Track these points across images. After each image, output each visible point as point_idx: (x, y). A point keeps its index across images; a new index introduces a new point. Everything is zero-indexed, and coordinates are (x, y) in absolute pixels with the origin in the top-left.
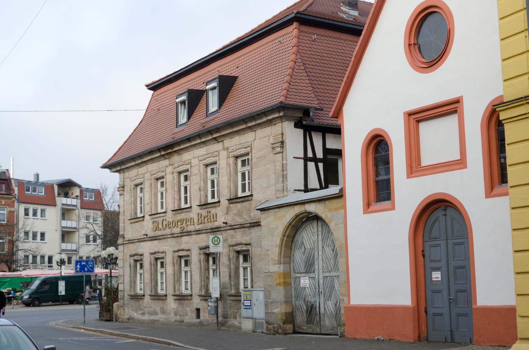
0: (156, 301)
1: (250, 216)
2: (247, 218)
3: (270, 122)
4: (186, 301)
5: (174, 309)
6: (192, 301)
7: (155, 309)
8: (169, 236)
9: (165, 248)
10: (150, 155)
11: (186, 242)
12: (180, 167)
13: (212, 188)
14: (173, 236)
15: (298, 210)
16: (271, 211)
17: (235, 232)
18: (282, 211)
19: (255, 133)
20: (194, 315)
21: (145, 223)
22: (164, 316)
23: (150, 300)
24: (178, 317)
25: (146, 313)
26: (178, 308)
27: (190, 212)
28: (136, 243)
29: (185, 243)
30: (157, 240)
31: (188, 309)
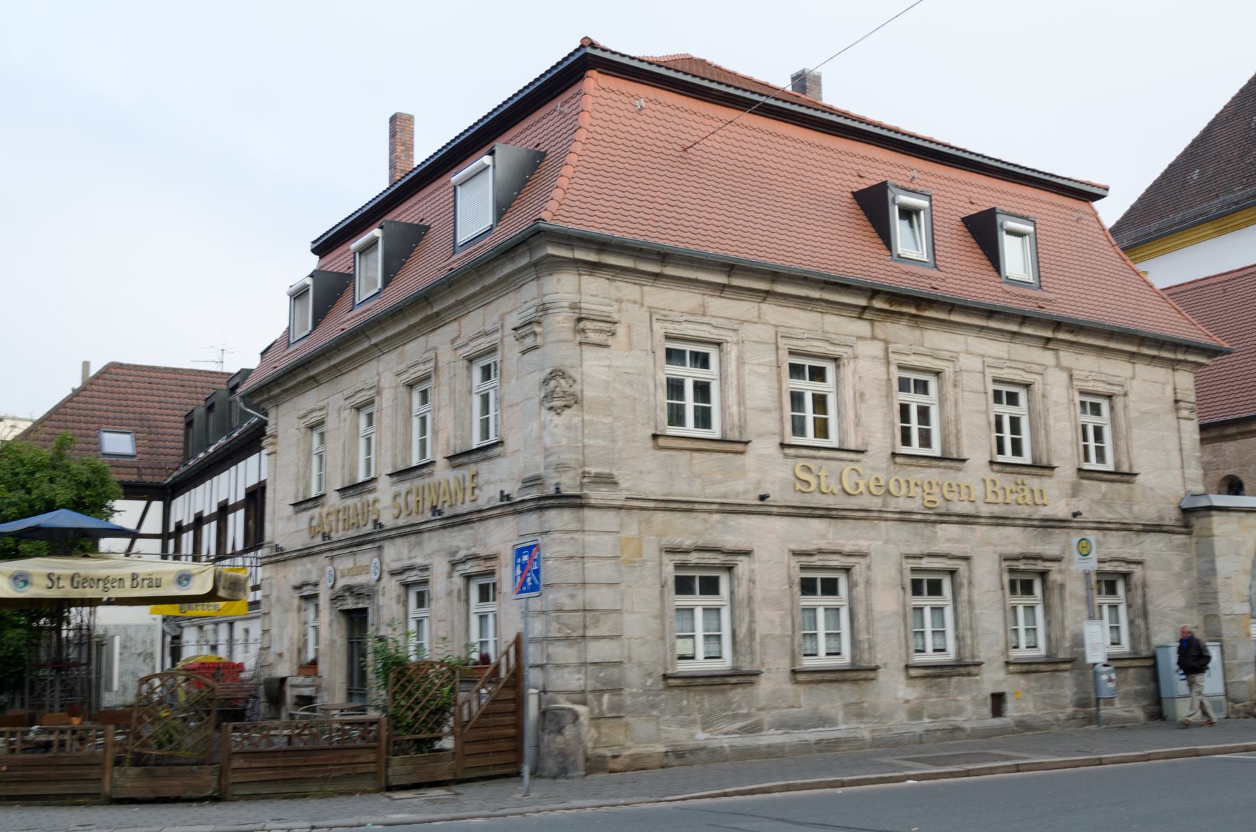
1: (1131, 511)
3: (1174, 364)
4: (955, 679)
5: (907, 701)
6: (977, 678)
8: (890, 516)
10: (822, 289)
11: (947, 538)
12: (913, 357)
13: (482, 415)
14: (905, 517)
17: (1105, 535)
19: (1134, 368)
20: (987, 710)
21: (749, 459)
22: (862, 726)
24: (926, 720)
25: (766, 727)
27: (959, 470)
28: (702, 516)
30: (827, 520)
31: (964, 699)
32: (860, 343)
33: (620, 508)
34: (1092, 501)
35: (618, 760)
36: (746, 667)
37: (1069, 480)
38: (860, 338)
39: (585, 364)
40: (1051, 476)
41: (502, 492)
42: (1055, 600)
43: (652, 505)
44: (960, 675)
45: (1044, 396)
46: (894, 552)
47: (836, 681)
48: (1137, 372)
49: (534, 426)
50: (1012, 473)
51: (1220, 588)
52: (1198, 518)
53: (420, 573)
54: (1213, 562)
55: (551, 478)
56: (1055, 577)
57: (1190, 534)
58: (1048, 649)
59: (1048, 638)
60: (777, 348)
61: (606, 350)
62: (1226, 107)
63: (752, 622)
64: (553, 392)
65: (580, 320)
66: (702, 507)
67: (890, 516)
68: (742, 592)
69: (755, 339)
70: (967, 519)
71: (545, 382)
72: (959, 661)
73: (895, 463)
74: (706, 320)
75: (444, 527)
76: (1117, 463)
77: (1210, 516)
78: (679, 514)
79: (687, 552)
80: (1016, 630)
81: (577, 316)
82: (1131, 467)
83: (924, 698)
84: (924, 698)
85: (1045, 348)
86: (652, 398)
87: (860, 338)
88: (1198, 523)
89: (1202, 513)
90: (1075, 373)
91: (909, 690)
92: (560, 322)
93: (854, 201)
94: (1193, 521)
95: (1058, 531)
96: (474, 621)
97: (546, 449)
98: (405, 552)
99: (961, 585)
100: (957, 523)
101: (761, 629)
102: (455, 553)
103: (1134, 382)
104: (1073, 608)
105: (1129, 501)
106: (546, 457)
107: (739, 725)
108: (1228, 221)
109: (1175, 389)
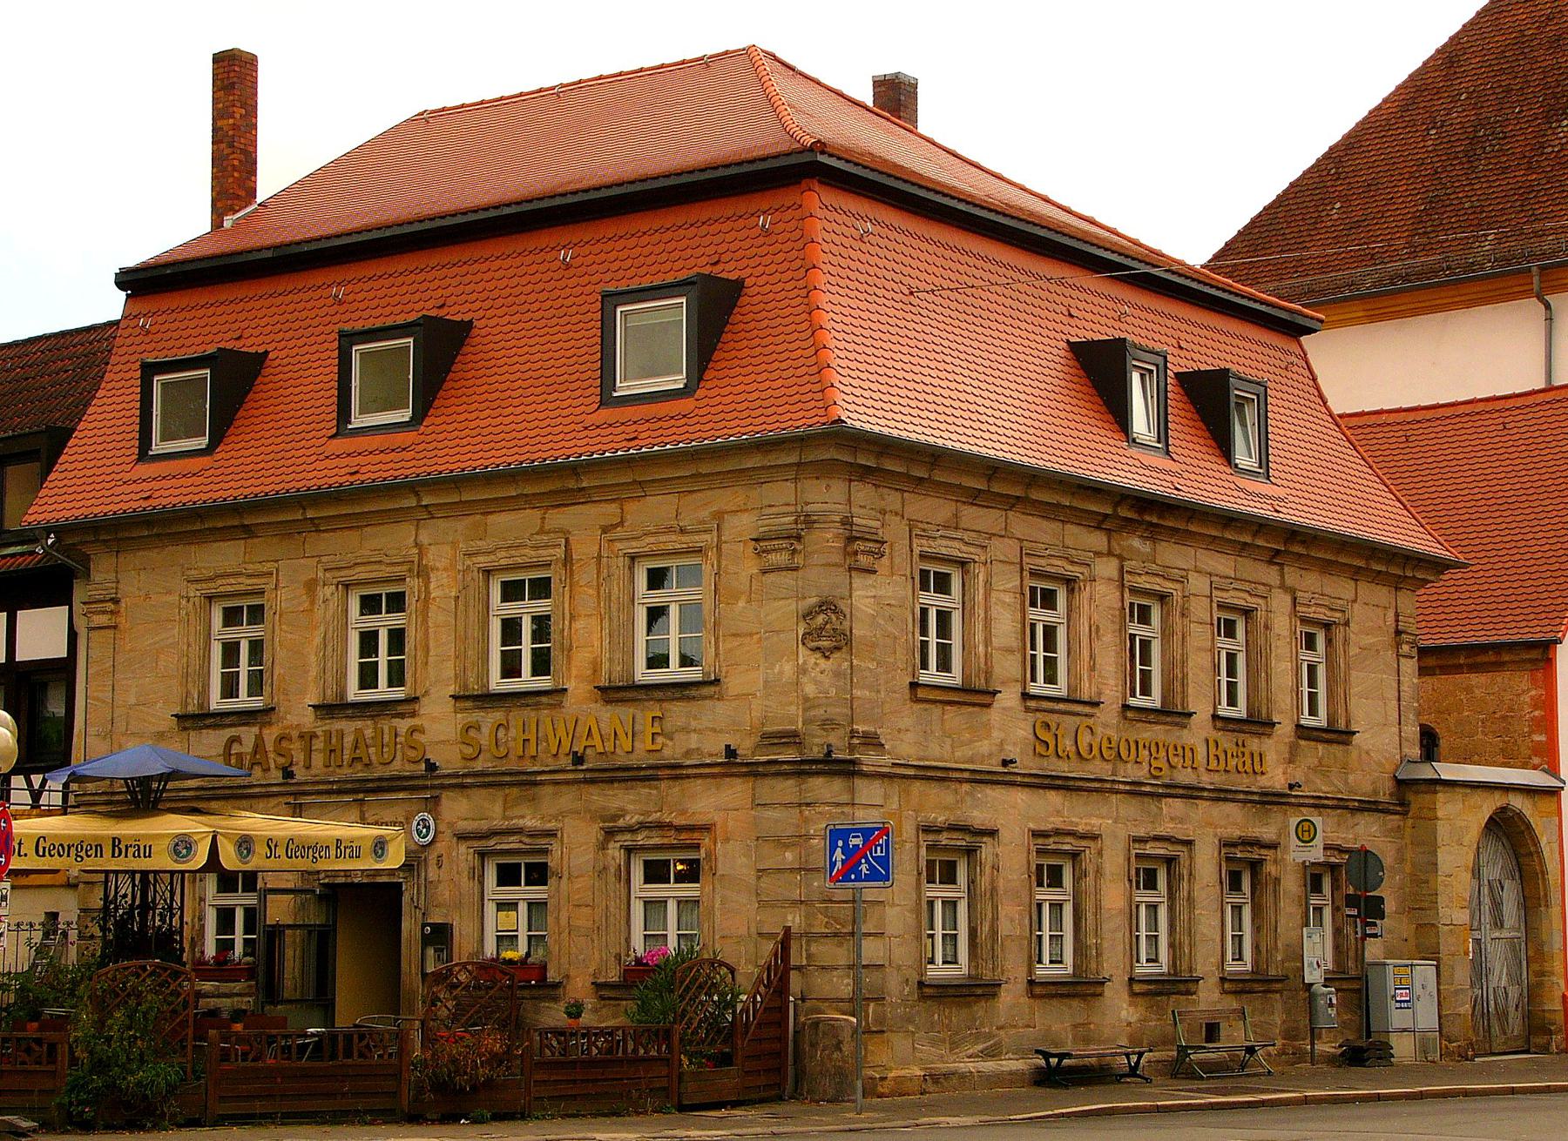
0: (1055, 1002)
1: (1346, 782)
2: (1341, 786)
5: (1129, 1024)
7: (1049, 1029)
8: (1122, 787)
9: (1094, 821)
11: (1172, 817)
14: (1135, 790)
15: (1498, 800)
16: (1457, 789)
18: (1477, 797)
21: (994, 715)
23: (1025, 1000)
26: (1143, 1020)
27: (1184, 727)
28: (953, 786)
29: (1172, 819)
32: (1097, 560)
33: (883, 776)
34: (1309, 768)
35: (886, 1083)
36: (988, 976)
37: (1287, 740)
38: (1098, 554)
39: (855, 594)
40: (1269, 736)
41: (728, 747)
42: (1268, 899)
43: (911, 772)
44: (1179, 993)
45: (1267, 627)
46: (1123, 833)
47: (1068, 996)
48: (1360, 592)
49: (788, 669)
50: (1234, 731)
51: (1440, 889)
52: (1417, 793)
53: (527, 840)
54: (1435, 852)
55: (814, 736)
56: (1270, 868)
57: (1405, 814)
58: (1256, 962)
59: (1256, 948)
60: (1022, 569)
61: (873, 577)
62: (1385, 101)
63: (995, 919)
64: (822, 629)
65: (851, 539)
66: (957, 775)
67: (1122, 787)
68: (984, 882)
69: (1002, 558)
70: (1191, 793)
71: (808, 615)
72: (1175, 974)
73: (1126, 718)
74: (959, 535)
75: (586, 781)
76: (1331, 718)
77: (1435, 792)
78: (934, 784)
79: (939, 831)
80: (932, 936)
81: (847, 533)
82: (1348, 723)
83: (1145, 1020)
84: (1145, 1020)
85: (1270, 562)
86: (910, 636)
87: (1098, 554)
88: (1417, 801)
89: (1423, 788)
90: (1299, 594)
91: (1131, 1009)
92: (826, 540)
93: (1069, 355)
94: (1410, 797)
95: (1275, 808)
96: (638, 910)
97: (806, 699)
98: (497, 809)
99: (1181, 877)
100: (1182, 796)
101: (1004, 928)
102: (615, 818)
103: (1356, 606)
104: (1288, 911)
105: (1345, 768)
106: (805, 710)
107: (980, 1047)
108: (1393, 302)
109: (1397, 615)
